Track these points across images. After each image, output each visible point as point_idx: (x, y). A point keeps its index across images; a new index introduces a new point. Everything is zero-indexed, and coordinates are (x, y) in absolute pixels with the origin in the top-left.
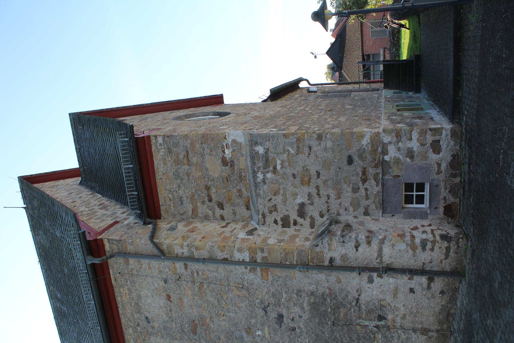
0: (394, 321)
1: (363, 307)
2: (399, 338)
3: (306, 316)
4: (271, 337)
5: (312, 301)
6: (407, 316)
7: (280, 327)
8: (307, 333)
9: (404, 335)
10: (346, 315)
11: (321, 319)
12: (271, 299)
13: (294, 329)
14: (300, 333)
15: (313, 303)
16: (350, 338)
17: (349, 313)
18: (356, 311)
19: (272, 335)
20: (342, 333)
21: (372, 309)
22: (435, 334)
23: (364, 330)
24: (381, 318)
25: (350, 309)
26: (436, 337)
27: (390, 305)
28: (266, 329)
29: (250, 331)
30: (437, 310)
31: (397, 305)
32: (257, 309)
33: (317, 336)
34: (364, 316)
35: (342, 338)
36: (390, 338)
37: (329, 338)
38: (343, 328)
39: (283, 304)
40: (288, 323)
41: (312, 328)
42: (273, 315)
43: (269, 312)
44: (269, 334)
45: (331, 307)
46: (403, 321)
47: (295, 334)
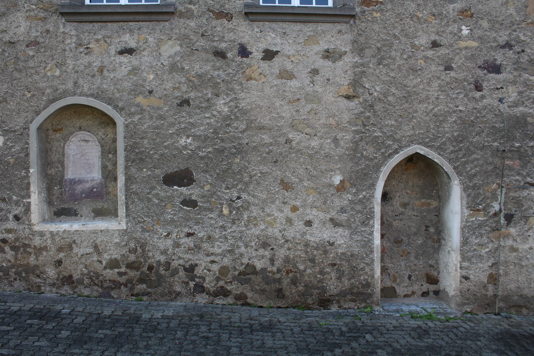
0: (507, 236)
1: (525, 193)
2: (480, 245)
3: (503, 108)
4: (461, 49)
5: (529, 119)
6: (515, 254)
7: (479, 67)
8: (476, 109)
9: (486, 252)
10: (511, 169)
11: (500, 131)
12: (527, 58)
13: (478, 88)
14: (474, 98)
15: (526, 121)
16: (475, 175)
17: (513, 173)
18: (518, 183)
19: (464, 52)
20: (481, 162)
21: (523, 205)
22: (490, 293)
23: (489, 194)
24: (509, 218)
25: (519, 174)
26: (487, 295)
27: (529, 230)
28: (475, 44)
29: (467, 16)
30: (526, 292)
31: (531, 239)
32: (507, 33)
33: (472, 124)
34: (512, 194)
35: (473, 162)
36: (480, 233)
37: (471, 143)
38: (490, 163)
39: (520, 76)
40: (488, 81)
41: (483, 117)
42: (499, 57)
43: (502, 51)
44: (466, 48)
45: (520, 147)
46: (507, 248)
47: (471, 90)
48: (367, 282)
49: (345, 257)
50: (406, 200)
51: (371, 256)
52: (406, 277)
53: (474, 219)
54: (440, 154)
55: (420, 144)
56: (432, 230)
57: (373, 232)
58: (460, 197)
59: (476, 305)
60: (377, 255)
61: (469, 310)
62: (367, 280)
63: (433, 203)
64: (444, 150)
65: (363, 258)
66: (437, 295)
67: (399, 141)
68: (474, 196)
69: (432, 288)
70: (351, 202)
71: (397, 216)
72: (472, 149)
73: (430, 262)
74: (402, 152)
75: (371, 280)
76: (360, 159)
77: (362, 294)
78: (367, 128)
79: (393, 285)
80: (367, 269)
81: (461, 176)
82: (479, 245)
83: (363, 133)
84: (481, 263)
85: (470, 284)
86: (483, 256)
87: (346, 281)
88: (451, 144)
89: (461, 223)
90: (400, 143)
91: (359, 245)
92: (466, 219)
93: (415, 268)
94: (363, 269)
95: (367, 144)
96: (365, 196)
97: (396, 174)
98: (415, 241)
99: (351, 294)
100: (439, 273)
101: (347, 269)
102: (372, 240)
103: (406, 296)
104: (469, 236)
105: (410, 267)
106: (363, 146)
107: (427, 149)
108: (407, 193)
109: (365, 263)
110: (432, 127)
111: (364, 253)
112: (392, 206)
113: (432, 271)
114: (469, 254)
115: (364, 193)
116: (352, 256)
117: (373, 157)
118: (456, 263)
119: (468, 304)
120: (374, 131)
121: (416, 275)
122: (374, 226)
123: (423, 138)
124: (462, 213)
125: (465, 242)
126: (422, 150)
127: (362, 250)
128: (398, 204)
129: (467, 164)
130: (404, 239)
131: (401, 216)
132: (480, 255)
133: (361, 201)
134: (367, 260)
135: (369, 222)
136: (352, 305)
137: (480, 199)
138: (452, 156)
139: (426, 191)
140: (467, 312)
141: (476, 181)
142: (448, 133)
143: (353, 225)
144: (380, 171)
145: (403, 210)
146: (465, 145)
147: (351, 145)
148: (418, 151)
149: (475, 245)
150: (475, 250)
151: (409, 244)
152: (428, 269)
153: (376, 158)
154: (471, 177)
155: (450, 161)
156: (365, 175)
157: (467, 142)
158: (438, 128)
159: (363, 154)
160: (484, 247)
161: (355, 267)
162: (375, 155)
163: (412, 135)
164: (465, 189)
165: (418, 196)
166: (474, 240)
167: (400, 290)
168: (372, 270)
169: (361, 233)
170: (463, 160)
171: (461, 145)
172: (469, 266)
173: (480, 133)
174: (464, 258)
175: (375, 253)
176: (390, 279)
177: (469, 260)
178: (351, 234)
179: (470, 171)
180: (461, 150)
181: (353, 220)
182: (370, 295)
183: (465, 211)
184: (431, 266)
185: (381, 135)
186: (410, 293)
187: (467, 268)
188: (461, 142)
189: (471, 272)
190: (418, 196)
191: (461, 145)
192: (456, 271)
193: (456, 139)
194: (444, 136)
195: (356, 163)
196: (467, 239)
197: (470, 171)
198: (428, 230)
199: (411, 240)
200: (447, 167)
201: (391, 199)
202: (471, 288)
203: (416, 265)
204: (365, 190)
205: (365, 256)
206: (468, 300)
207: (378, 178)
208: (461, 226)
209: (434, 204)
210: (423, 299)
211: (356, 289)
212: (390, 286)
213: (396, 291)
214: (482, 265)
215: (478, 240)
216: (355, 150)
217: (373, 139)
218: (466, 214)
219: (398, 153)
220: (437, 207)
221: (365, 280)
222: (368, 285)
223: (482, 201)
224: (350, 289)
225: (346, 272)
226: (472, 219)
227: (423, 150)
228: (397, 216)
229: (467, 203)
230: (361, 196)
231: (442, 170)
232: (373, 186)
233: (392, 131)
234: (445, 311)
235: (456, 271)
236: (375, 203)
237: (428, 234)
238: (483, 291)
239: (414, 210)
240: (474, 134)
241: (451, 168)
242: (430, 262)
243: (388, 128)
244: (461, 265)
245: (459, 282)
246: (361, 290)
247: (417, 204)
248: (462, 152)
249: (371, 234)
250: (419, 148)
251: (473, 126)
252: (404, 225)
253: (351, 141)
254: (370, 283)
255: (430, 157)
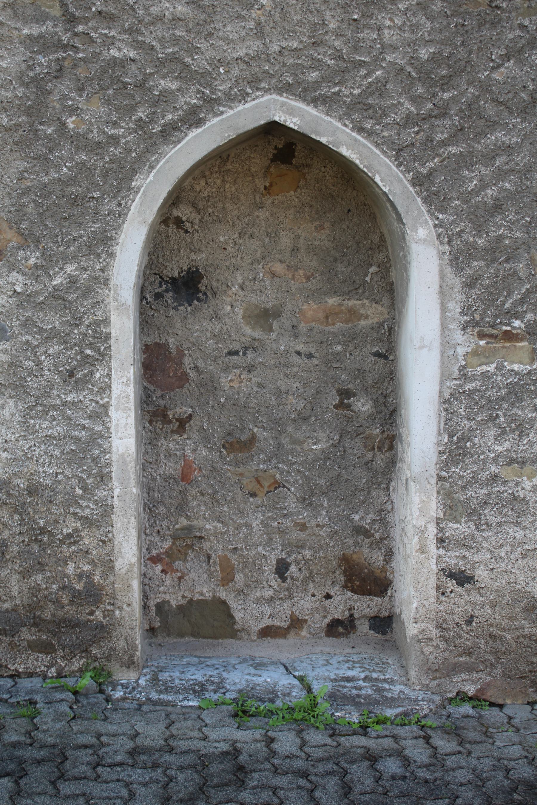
16: (498, 207)
20: (522, 159)
37: (485, 87)
48: (90, 583)
49: (9, 495)
50: (269, 298)
51: (100, 493)
52: (269, 568)
53: (492, 368)
54: (360, 130)
55: (285, 89)
56: (363, 405)
57: (106, 407)
58: (436, 287)
59: (498, 672)
60: (124, 491)
61: (470, 689)
62: (89, 576)
63: (370, 312)
64: (380, 115)
65: (73, 501)
66: (384, 633)
67: (204, 78)
68: (494, 285)
69: (366, 606)
70: (23, 299)
71: (236, 353)
72: (490, 109)
73: (356, 517)
74: (215, 120)
75: (104, 576)
76: (52, 144)
77: (74, 625)
78: (80, 28)
79: (223, 594)
80: (88, 540)
81: (442, 209)
82: (511, 462)
83: (65, 47)
84: (517, 524)
85: (474, 597)
86: (524, 501)
87: (16, 577)
88: (406, 90)
89: (442, 382)
90: (209, 85)
91: (57, 452)
92: (462, 368)
93: (303, 535)
94: (72, 538)
95: (80, 90)
96: (73, 281)
97: (230, 206)
98: (301, 443)
99: (35, 624)
100: (389, 555)
101: (18, 539)
102: (105, 435)
103: (267, 632)
104: (471, 430)
105: (282, 532)
106: (64, 98)
107: (310, 110)
108: (273, 275)
109: (81, 518)
110: (333, 25)
111: (74, 481)
112: (218, 317)
113: (366, 550)
114: (470, 493)
115: (70, 268)
116: (33, 490)
117: (101, 139)
118: (421, 523)
119: (470, 669)
120: (109, 42)
121: (307, 561)
122: (109, 387)
123: (297, 70)
124: (446, 344)
125: (456, 449)
126: (291, 112)
127: (68, 472)
128: (240, 312)
129: (470, 167)
130: (261, 434)
131: (250, 355)
132: (515, 498)
133: (58, 297)
134: (88, 508)
135: (91, 373)
136: (38, 662)
137: (516, 296)
138: (409, 135)
139: (340, 267)
140: (462, 697)
141: (499, 227)
142: (394, 48)
143: (32, 384)
144: (129, 189)
145: (258, 334)
146: (463, 94)
147: (20, 92)
148: (279, 117)
149: (495, 460)
150: (494, 478)
151: (278, 454)
152: (350, 541)
153: (115, 140)
154: (482, 216)
155: (400, 153)
156: (75, 201)
157: (470, 83)
158: (357, 30)
159: (64, 124)
160: (528, 468)
161: (43, 531)
162: (110, 131)
163: (256, 57)
164: (458, 258)
165: (313, 284)
166: (491, 444)
167: (248, 613)
168: (106, 541)
169: (63, 413)
170: (453, 150)
171: (446, 96)
172: (472, 537)
173: (520, 51)
174: (453, 506)
175: (115, 483)
176: (211, 575)
177: (473, 514)
178: (28, 413)
179: (476, 191)
180: (444, 115)
181: (30, 364)
182: (103, 631)
183: (459, 337)
184: (360, 531)
185: (132, 54)
186: (282, 622)
187: (463, 544)
188: (446, 83)
189: (477, 558)
190: (313, 284)
191: (446, 96)
192: (422, 550)
193: (425, 74)
194: (377, 60)
195: (37, 158)
196: (464, 439)
197: (476, 191)
198: (348, 407)
199: (286, 441)
200: (388, 176)
201: (214, 294)
202: (477, 613)
203: (303, 527)
204: (75, 257)
205: (79, 491)
206: (470, 654)
207: (122, 215)
208: (441, 393)
209: (373, 313)
210: (329, 644)
211: (51, 607)
212: (208, 596)
213: (232, 617)
214: (519, 534)
215: (507, 445)
216: (35, 110)
217: (104, 71)
218: (461, 351)
219: (199, 123)
220: (381, 324)
221: (80, 577)
222: (93, 595)
223: (522, 301)
224: (31, 608)
225: (14, 549)
226: (484, 368)
227: (297, 115)
228: (236, 353)
229: (466, 310)
230: (58, 281)
231: (377, 190)
232: (102, 244)
233: (176, 40)
234: (379, 690)
235: (422, 550)
236: (113, 304)
237: (349, 419)
238: (526, 624)
239: (296, 336)
240: (496, 53)
241: (405, 180)
242: (356, 517)
243: (160, 31)
244: (441, 530)
245: (433, 593)
246: (70, 611)
247: (310, 314)
248: (447, 122)
249: (101, 413)
250: (283, 105)
251: (493, 24)
252: (260, 385)
253: (20, 78)
254: (101, 588)
255: (324, 140)
